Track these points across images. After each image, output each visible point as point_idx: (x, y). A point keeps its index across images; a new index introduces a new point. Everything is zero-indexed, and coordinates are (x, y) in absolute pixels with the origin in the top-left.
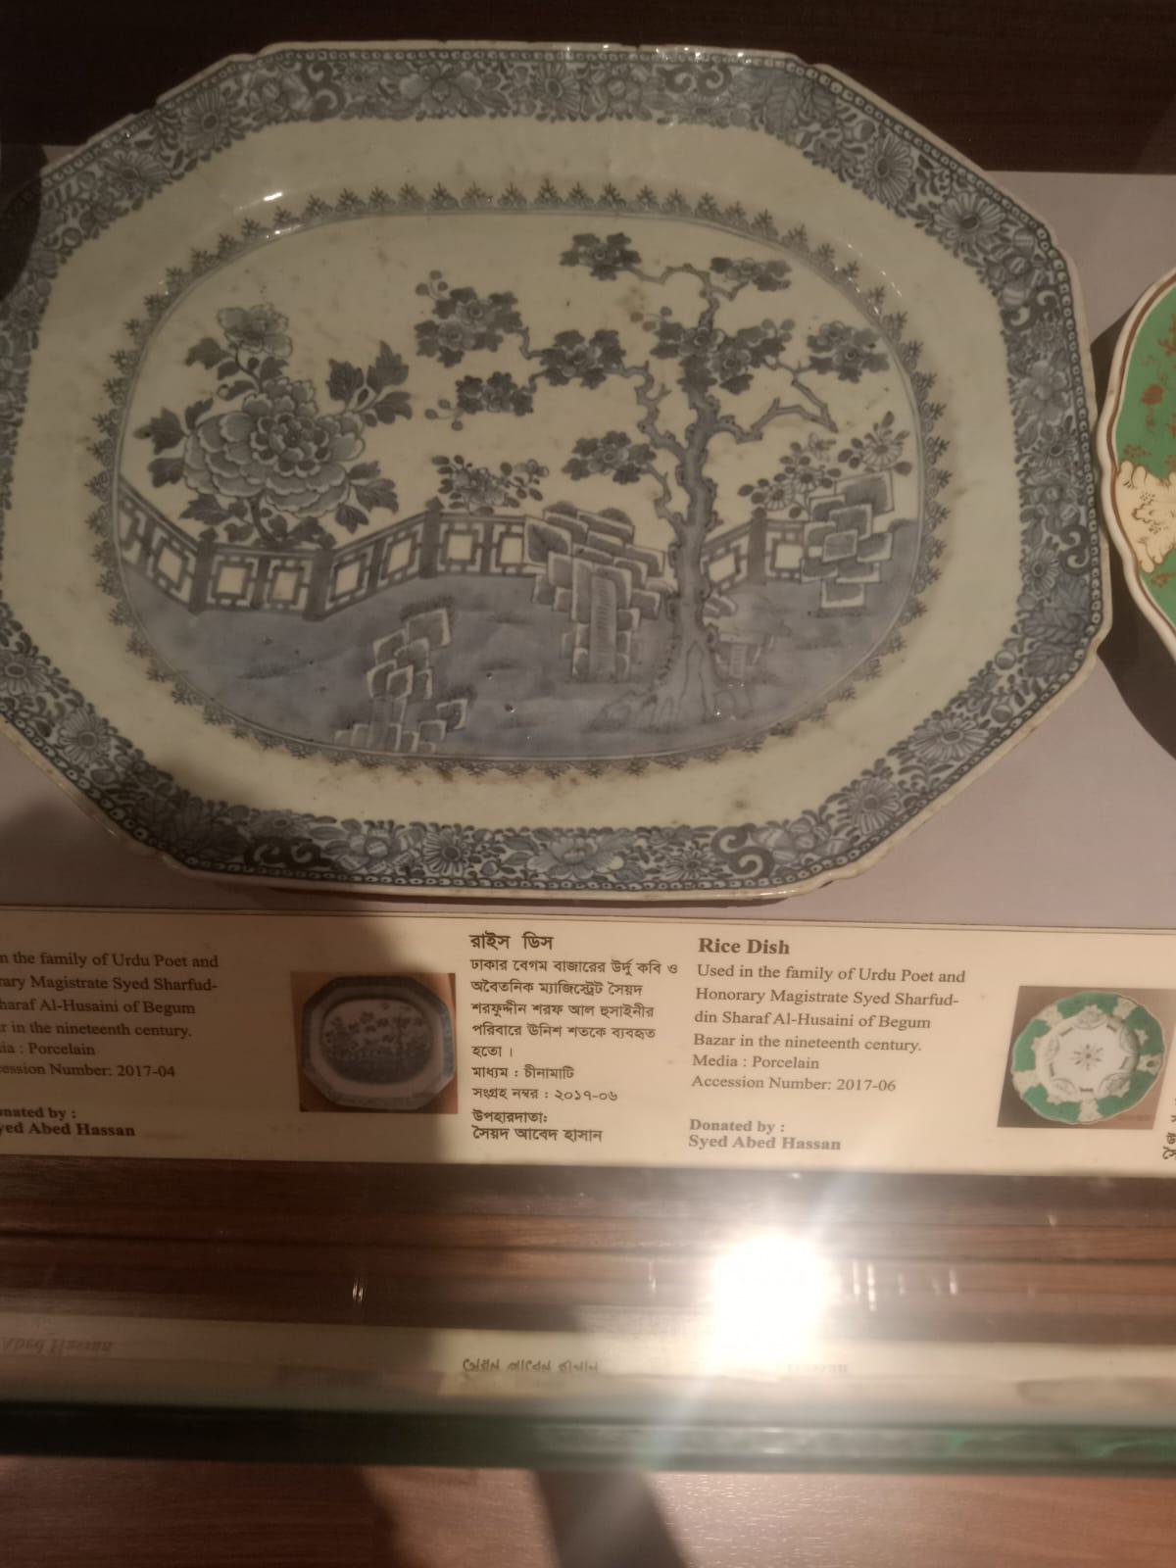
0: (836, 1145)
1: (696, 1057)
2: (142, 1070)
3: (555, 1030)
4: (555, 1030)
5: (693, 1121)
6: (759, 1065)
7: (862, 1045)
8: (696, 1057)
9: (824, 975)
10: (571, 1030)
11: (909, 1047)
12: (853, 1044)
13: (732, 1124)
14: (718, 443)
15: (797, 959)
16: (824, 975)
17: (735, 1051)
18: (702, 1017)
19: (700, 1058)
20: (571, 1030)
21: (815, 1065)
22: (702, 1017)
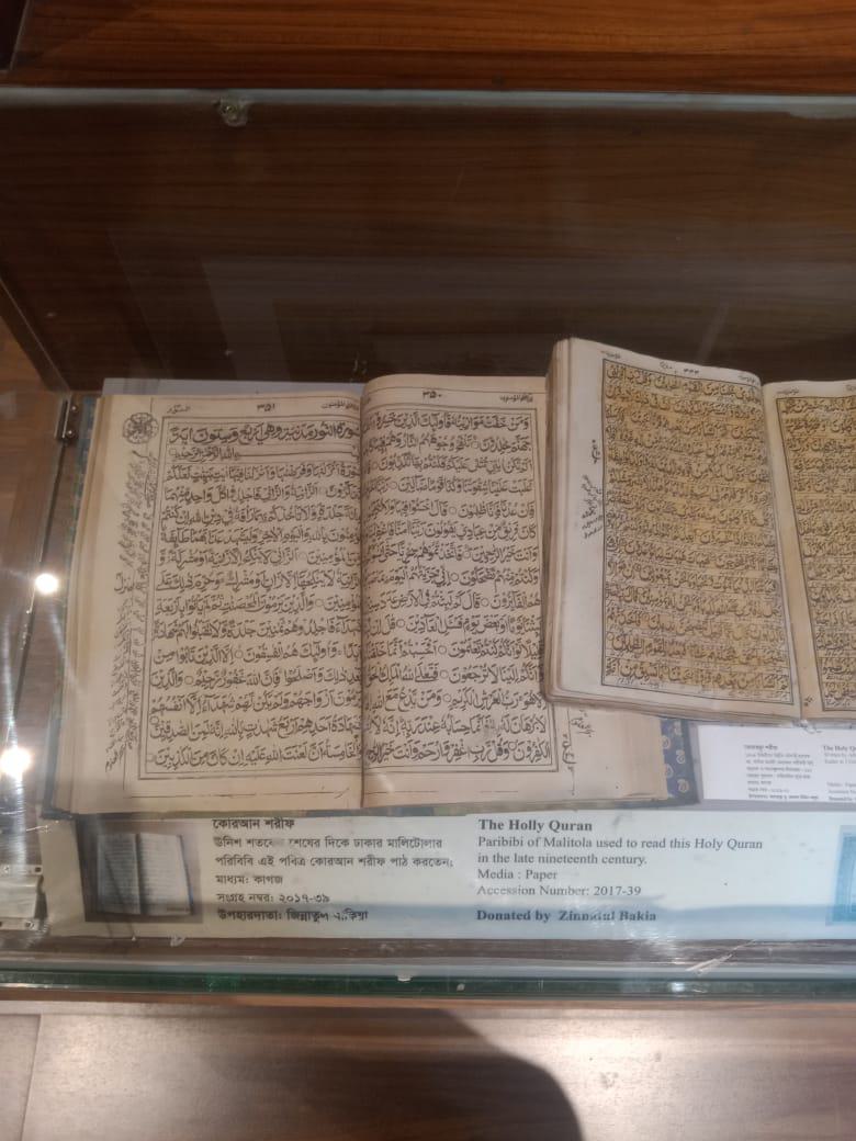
0: (439, 843)
1: (480, 872)
2: (614, 890)
3: (236, 842)
4: (236, 842)
5: (479, 912)
6: (531, 877)
7: (600, 860)
8: (480, 872)
9: (537, 827)
10: (249, 842)
11: (637, 861)
12: (592, 859)
13: (513, 914)
14: (359, 690)
15: (559, 883)
16: (537, 827)
17: (510, 867)
18: (483, 859)
19: (484, 872)
20: (249, 842)
21: (589, 827)
22: (483, 859)
